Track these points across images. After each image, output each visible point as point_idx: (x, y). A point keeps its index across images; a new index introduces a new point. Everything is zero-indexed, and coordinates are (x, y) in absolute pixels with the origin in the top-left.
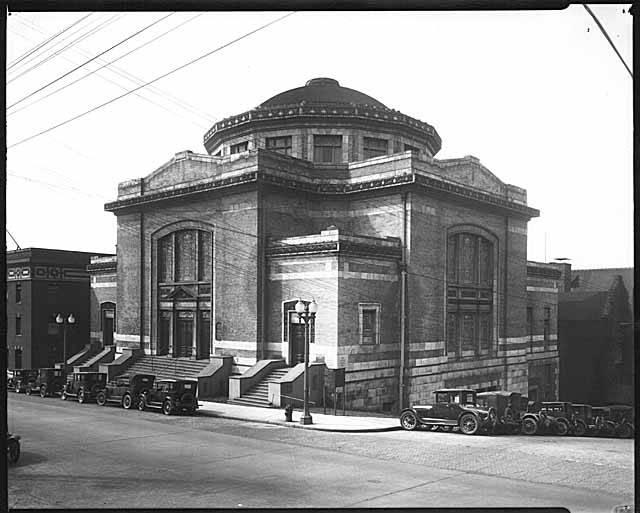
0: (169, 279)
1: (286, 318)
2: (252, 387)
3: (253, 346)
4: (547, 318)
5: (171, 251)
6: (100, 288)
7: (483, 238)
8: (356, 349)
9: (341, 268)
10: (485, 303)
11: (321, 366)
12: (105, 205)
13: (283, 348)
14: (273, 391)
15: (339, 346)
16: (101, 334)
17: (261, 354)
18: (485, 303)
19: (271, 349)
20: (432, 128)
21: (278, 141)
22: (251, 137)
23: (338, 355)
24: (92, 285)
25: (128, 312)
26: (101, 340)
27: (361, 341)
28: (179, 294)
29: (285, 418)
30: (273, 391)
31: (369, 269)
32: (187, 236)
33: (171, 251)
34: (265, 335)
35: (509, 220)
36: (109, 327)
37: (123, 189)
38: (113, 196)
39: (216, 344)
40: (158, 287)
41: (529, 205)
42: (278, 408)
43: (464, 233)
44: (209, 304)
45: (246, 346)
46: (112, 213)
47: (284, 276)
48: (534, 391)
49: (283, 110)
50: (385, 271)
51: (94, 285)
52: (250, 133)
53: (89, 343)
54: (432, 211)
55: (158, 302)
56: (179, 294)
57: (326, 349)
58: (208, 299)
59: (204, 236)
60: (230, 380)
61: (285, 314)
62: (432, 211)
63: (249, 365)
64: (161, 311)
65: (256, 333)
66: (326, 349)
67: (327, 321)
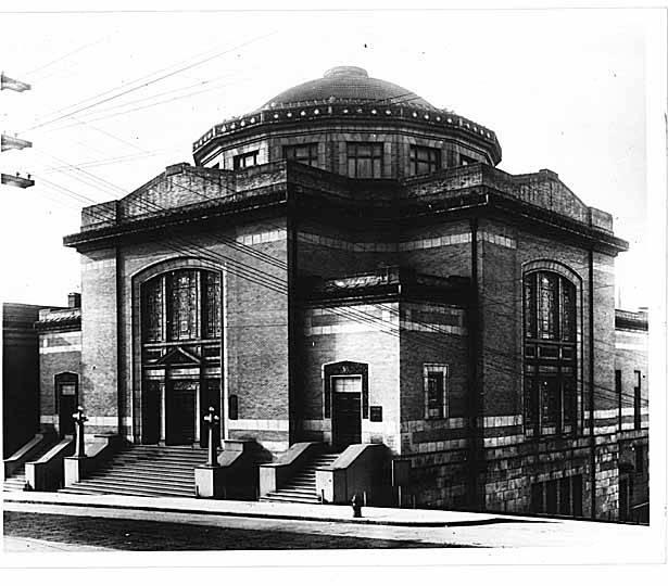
0: (161, 344)
1: (327, 387)
2: (293, 477)
3: (284, 426)
4: (637, 385)
5: (162, 298)
6: (53, 355)
7: (564, 278)
8: (420, 425)
9: (402, 317)
10: (566, 364)
11: (378, 449)
12: (64, 239)
13: (325, 425)
14: (323, 481)
15: (401, 421)
16: (57, 418)
17: (295, 436)
18: (566, 364)
19: (308, 428)
20: (492, 133)
21: (298, 150)
22: (264, 145)
23: (401, 432)
24: (41, 351)
25: (100, 381)
26: (57, 426)
27: (427, 416)
28: (173, 359)
29: (352, 512)
30: (323, 481)
31: (437, 319)
32: (184, 280)
33: (162, 298)
34: (300, 411)
35: (595, 254)
36: (69, 406)
37: (87, 212)
38: (75, 226)
39: (229, 424)
40: (143, 348)
41: (615, 235)
42: (331, 504)
43: (542, 272)
44: (219, 371)
45: (31, 508)
46: (75, 249)
47: (318, 330)
48: (625, 480)
49: (307, 109)
50: (451, 321)
51: (44, 350)
52: (261, 140)
53: (39, 431)
54: (508, 243)
55: (144, 369)
56: (173, 359)
57: (387, 430)
58: (216, 364)
59: (209, 279)
60: (261, 469)
61: (327, 380)
62: (508, 243)
63: (283, 451)
64: (147, 382)
65: (287, 407)
66: (387, 430)
67: (386, 390)
